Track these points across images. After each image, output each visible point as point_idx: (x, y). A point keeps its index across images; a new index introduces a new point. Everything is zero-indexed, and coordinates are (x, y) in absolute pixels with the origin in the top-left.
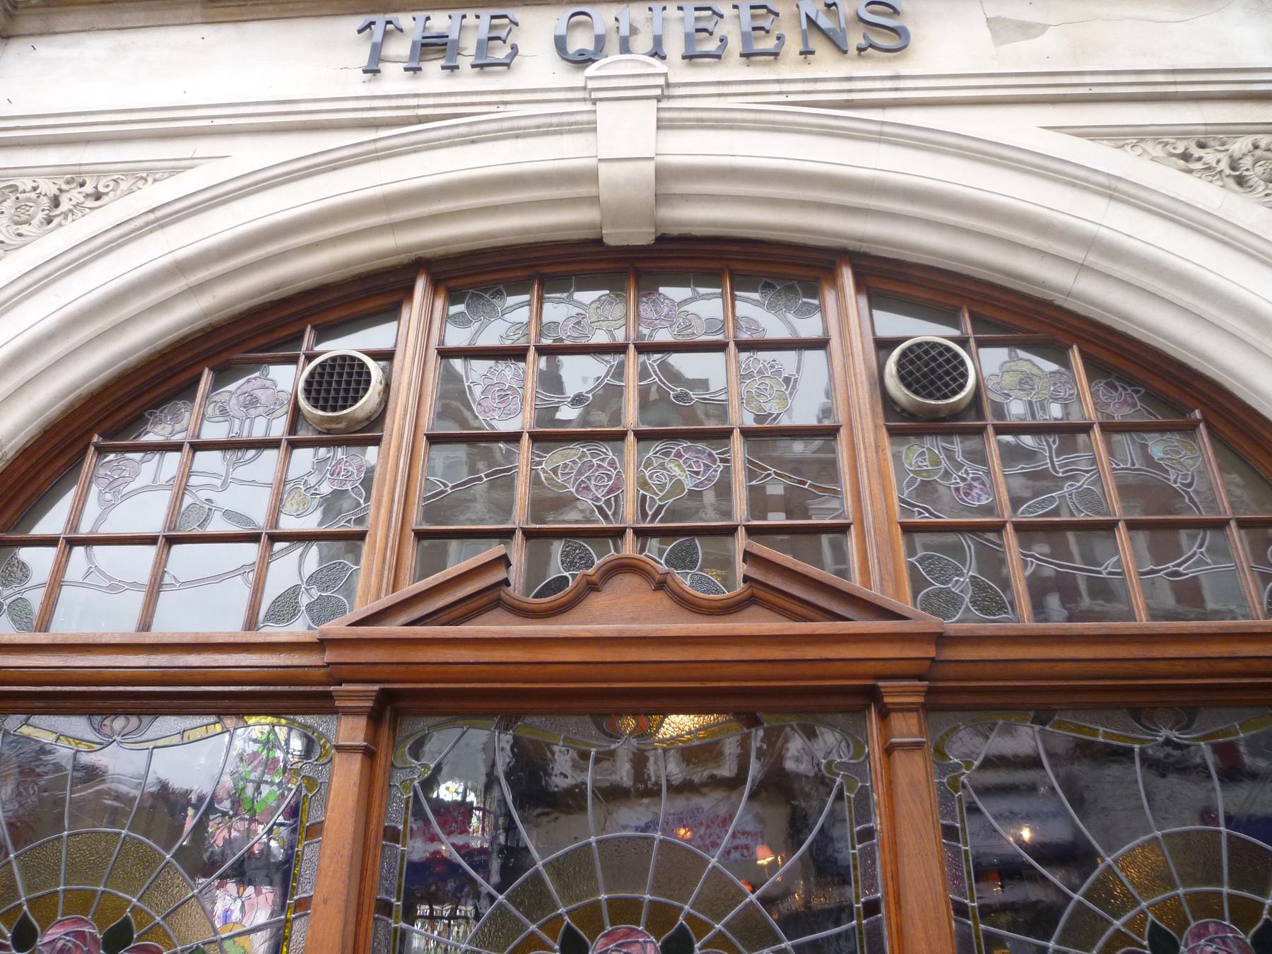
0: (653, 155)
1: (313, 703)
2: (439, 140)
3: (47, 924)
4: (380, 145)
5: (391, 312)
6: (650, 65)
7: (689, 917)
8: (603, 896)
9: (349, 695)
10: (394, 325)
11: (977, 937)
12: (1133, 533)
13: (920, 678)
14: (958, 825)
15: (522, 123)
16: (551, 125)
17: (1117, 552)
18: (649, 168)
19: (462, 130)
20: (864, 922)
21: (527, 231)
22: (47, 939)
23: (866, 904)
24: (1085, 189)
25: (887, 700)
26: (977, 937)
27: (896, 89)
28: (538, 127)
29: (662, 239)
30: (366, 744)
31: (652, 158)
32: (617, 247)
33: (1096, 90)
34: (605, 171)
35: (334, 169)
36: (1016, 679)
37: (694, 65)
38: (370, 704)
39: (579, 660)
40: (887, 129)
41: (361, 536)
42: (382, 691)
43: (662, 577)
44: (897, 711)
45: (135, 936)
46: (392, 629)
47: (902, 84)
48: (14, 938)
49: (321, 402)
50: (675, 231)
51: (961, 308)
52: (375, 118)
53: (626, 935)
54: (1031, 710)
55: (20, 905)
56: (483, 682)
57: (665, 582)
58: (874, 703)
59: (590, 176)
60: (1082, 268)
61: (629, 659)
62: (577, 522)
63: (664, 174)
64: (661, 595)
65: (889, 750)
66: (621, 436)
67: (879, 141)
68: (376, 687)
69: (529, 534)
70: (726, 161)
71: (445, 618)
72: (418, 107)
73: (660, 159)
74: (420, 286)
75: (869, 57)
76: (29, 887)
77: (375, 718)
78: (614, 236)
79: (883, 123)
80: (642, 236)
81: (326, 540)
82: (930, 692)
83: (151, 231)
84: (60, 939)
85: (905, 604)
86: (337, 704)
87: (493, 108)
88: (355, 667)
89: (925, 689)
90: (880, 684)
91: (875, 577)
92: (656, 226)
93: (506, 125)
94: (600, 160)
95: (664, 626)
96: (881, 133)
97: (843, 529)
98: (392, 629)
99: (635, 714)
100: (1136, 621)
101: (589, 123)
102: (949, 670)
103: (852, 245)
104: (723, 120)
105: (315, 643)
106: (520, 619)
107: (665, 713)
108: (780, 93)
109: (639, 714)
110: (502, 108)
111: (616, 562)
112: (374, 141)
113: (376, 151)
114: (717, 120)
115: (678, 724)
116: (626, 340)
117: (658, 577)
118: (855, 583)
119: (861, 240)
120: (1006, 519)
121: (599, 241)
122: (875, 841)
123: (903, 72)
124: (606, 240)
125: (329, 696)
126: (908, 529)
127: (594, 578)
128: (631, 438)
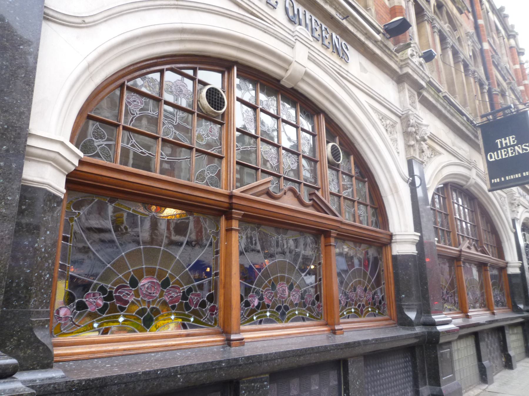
2: (258, 26)
3: (141, 277)
4: (245, 18)
6: (309, 36)
7: (170, 274)
8: (144, 266)
9: (236, 214)
12: (262, 173)
15: (279, 35)
16: (285, 40)
18: (304, 70)
19: (265, 27)
20: (214, 277)
21: (267, 69)
22: (142, 284)
23: (215, 273)
24: (370, 121)
27: (347, 75)
28: (282, 38)
29: (292, 89)
33: (374, 96)
34: (294, 65)
35: (230, 18)
36: (280, 219)
37: (323, 47)
40: (346, 87)
42: (244, 214)
44: (234, 219)
45: (171, 283)
47: (349, 74)
48: (130, 283)
49: (217, 108)
52: (241, 4)
53: (282, 284)
54: (108, 197)
55: (130, 272)
59: (289, 63)
60: (364, 140)
61: (261, 208)
63: (307, 74)
67: (342, 88)
70: (317, 77)
72: (253, 8)
75: (342, 60)
78: (284, 82)
79: (345, 85)
80: (288, 84)
81: (185, 148)
82: (244, 215)
83: (173, 8)
84: (146, 284)
87: (272, 23)
92: (296, 85)
93: (275, 33)
95: (291, 206)
96: (344, 87)
97: (221, 158)
99: (156, 205)
100: (156, 173)
101: (293, 45)
103: (327, 111)
104: (318, 63)
106: (269, 198)
107: (166, 207)
108: (329, 62)
109: (158, 206)
110: (274, 25)
112: (244, 15)
113: (242, 19)
114: (317, 63)
115: (169, 212)
119: (330, 112)
120: (224, 156)
121: (279, 81)
123: (343, 66)
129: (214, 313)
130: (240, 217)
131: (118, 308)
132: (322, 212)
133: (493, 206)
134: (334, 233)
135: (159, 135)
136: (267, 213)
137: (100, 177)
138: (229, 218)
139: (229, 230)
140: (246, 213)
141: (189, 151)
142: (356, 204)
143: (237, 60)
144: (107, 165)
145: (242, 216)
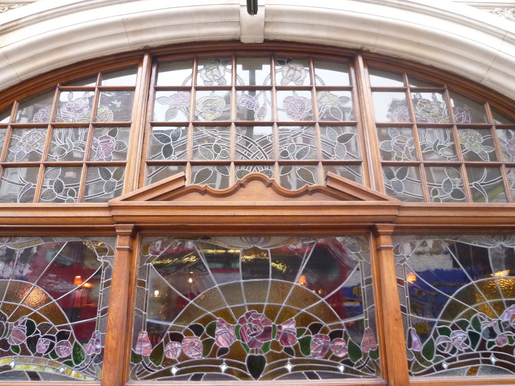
0: (264, 4)
1: (29, 232)
5: (133, 69)
10: (136, 75)
11: (145, 323)
13: (391, 222)
14: (146, 281)
17: (500, 174)
25: (379, 231)
26: (145, 323)
30: (129, 247)
31: (264, 6)
32: (248, 44)
38: (131, 231)
39: (461, 216)
41: (124, 165)
43: (271, 182)
46: (141, 202)
50: (272, 38)
51: (404, 73)
56: (63, 225)
57: (272, 184)
58: (373, 232)
62: (435, 160)
64: (270, 189)
65: (378, 250)
66: (229, 124)
68: (133, 225)
69: (281, 164)
71: (166, 197)
73: (267, 7)
74: (146, 59)
76: (506, 295)
77: (133, 236)
78: (246, 39)
80: (259, 39)
85: (383, 194)
86: (117, 231)
88: (387, 217)
89: (132, 227)
90: (377, 224)
91: (373, 184)
94: (241, 5)
97: (359, 163)
98: (141, 202)
102: (401, 219)
105: (107, 207)
111: (259, 175)
116: (271, 84)
117: (268, 182)
118: (364, 186)
120: (462, 162)
121: (239, 41)
122: (372, 284)
124: (242, 41)
125: (114, 229)
126: (383, 165)
127: (243, 182)
128: (233, 125)
129: (356, 363)
130: (392, 231)
131: (295, 353)
132: (347, 198)
133: (286, 19)
134: (382, 229)
135: (419, 161)
136: (33, 221)
137: (298, 218)
138: (377, 235)
139: (378, 250)
140: (398, 225)
141: (455, 170)
142: (422, 169)
143: (145, 45)
144: (68, 206)
145: (393, 229)
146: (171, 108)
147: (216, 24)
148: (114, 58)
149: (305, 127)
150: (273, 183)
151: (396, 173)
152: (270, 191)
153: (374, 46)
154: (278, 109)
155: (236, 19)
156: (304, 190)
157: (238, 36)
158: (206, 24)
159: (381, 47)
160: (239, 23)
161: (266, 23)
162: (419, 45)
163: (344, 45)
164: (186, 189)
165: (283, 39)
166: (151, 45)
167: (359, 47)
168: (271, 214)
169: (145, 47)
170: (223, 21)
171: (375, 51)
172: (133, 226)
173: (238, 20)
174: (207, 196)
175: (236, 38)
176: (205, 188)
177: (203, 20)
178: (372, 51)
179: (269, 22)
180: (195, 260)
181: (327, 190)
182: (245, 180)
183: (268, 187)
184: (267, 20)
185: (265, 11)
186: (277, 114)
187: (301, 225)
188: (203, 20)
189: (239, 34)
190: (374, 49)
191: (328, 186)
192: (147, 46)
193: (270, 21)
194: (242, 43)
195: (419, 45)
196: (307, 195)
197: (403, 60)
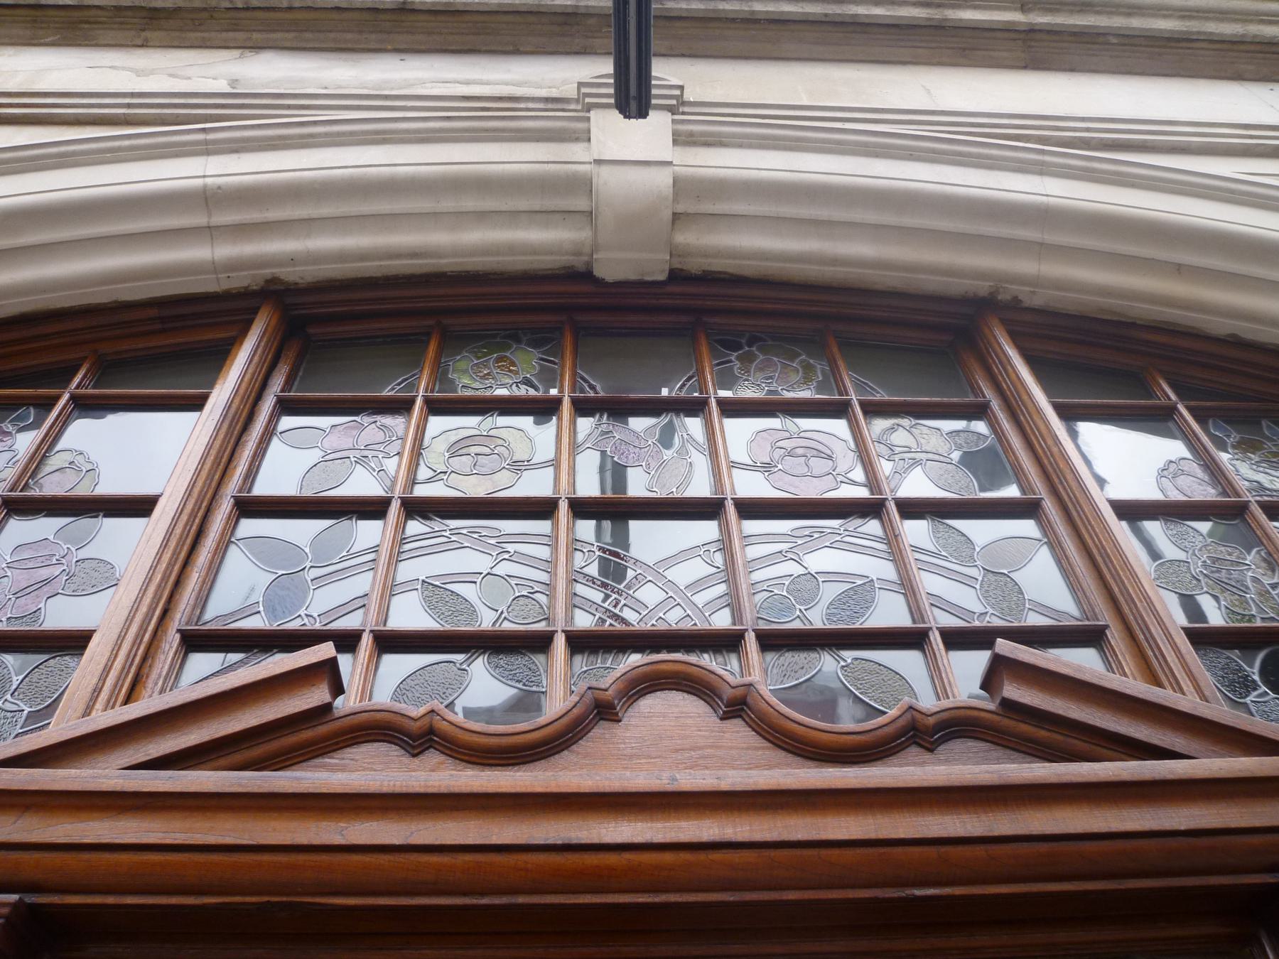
50: (695, 265)
64: (737, 726)
78: (612, 267)
117: (728, 693)
121: (585, 276)
124: (599, 272)
143: (268, 272)
146: (327, 458)
147: (513, 217)
148: (153, 312)
149: (754, 733)
150: (749, 700)
151: (1256, 670)
152: (738, 732)
153: (1035, 282)
154: (733, 465)
155: (581, 204)
156: (901, 722)
157: (586, 258)
158: (482, 217)
159: (1059, 285)
160: (589, 215)
161: (676, 216)
162: (1179, 270)
163: (932, 284)
164: (337, 724)
165: (730, 270)
166: (289, 274)
167: (983, 288)
168: (758, 837)
169: (268, 281)
170: (537, 208)
171: (1037, 302)
172: (15, 906)
173: (587, 208)
174: (433, 757)
175: (579, 263)
176: (426, 720)
177: (470, 203)
178: (1028, 301)
179: (687, 215)
180: (36, 488)
181: (1006, 723)
182: (620, 685)
183: (724, 718)
184: (680, 208)
185: (675, 181)
186: (730, 476)
187: (918, 892)
188: (470, 203)
189: (587, 250)
190: (1033, 293)
191: (1009, 706)
192: (274, 280)
193: (690, 211)
194: (599, 282)
195: (1179, 270)
196: (914, 750)
197: (1133, 325)
